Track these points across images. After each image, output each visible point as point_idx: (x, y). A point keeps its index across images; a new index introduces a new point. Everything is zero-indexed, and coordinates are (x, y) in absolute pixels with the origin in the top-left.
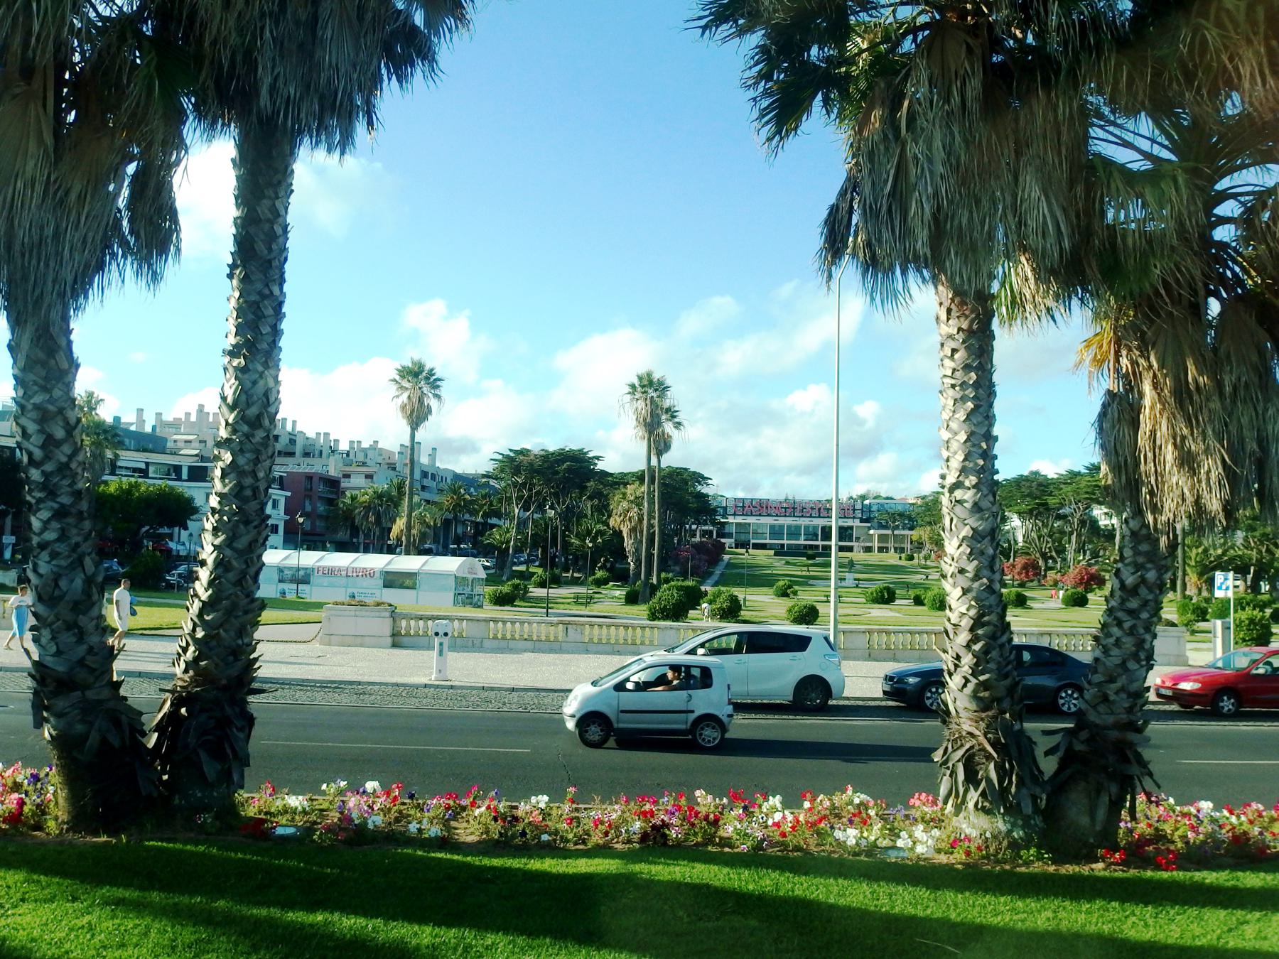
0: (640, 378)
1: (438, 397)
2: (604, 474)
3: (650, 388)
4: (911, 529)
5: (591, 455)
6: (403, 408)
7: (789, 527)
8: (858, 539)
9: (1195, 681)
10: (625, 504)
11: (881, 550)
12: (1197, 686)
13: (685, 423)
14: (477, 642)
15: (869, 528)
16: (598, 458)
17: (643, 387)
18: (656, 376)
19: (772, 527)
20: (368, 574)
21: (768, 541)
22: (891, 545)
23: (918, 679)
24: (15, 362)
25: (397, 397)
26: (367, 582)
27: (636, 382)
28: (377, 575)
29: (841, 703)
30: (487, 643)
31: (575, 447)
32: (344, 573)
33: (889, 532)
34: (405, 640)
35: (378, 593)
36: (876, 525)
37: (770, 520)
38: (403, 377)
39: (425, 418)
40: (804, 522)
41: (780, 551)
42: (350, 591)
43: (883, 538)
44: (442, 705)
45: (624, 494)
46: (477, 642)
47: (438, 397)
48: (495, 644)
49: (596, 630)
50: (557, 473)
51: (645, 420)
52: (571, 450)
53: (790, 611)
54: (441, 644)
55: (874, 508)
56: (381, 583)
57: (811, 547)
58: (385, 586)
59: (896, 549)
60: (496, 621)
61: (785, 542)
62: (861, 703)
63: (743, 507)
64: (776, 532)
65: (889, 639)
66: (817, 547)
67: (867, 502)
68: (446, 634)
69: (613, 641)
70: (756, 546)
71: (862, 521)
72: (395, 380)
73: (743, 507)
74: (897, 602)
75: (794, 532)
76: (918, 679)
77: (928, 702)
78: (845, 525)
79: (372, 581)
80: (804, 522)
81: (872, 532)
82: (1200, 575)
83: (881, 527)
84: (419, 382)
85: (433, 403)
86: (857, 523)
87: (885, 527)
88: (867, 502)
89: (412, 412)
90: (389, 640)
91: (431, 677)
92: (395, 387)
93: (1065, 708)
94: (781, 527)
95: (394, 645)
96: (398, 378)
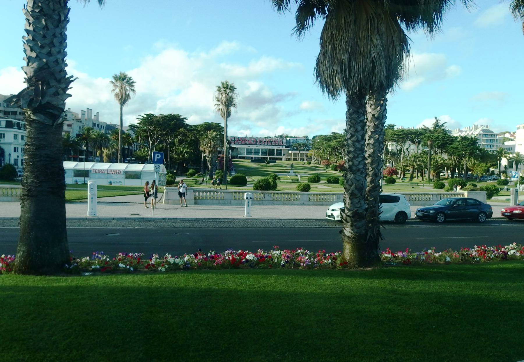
0: (223, 84)
1: (133, 90)
2: (188, 125)
3: (227, 89)
4: (307, 150)
5: (182, 117)
6: (117, 95)
7: (255, 149)
8: (284, 155)
9: (520, 210)
10: (207, 140)
11: (294, 159)
12: (520, 212)
13: (237, 104)
14: (229, 201)
15: (289, 150)
16: (185, 118)
17: (224, 88)
18: (230, 84)
19: (247, 149)
20: (117, 172)
21: (245, 156)
22: (299, 157)
23: (434, 211)
24: (348, 111)
25: (113, 90)
26: (115, 176)
27: (221, 85)
28: (122, 173)
29: (410, 221)
30: (233, 202)
31: (175, 114)
32: (106, 172)
33: (298, 152)
34: (199, 201)
35: (122, 181)
36: (292, 149)
37: (246, 147)
38: (116, 81)
39: (127, 100)
40: (261, 147)
41: (254, 160)
42: (109, 180)
43: (295, 155)
44: (136, 226)
45: (207, 135)
46: (229, 201)
47: (133, 90)
48: (236, 202)
49: (276, 195)
50: (169, 125)
51: (225, 103)
52: (174, 115)
53: (299, 186)
54: (248, 202)
55: (291, 141)
56: (124, 176)
57: (264, 158)
58: (127, 178)
59: (301, 159)
60: (236, 192)
61: (253, 156)
62: (497, 220)
63: (235, 140)
64: (249, 152)
65: (294, 197)
66: (267, 158)
67: (288, 139)
68: (251, 198)
69: (219, 198)
70: (240, 158)
71: (286, 147)
72: (112, 82)
73: (235, 140)
74: (321, 182)
75: (257, 152)
76: (434, 211)
77: (438, 219)
78: (279, 148)
79: (119, 176)
80: (261, 147)
81: (290, 152)
82: (434, 171)
83: (294, 149)
84: (227, 94)
85: (131, 93)
86: (284, 148)
87: (297, 150)
88: (288, 139)
89: (122, 97)
90: (194, 201)
91: (245, 216)
92: (112, 85)
93: (440, 221)
94: (251, 149)
95: (196, 204)
96: (114, 81)
